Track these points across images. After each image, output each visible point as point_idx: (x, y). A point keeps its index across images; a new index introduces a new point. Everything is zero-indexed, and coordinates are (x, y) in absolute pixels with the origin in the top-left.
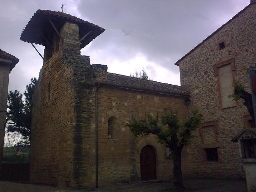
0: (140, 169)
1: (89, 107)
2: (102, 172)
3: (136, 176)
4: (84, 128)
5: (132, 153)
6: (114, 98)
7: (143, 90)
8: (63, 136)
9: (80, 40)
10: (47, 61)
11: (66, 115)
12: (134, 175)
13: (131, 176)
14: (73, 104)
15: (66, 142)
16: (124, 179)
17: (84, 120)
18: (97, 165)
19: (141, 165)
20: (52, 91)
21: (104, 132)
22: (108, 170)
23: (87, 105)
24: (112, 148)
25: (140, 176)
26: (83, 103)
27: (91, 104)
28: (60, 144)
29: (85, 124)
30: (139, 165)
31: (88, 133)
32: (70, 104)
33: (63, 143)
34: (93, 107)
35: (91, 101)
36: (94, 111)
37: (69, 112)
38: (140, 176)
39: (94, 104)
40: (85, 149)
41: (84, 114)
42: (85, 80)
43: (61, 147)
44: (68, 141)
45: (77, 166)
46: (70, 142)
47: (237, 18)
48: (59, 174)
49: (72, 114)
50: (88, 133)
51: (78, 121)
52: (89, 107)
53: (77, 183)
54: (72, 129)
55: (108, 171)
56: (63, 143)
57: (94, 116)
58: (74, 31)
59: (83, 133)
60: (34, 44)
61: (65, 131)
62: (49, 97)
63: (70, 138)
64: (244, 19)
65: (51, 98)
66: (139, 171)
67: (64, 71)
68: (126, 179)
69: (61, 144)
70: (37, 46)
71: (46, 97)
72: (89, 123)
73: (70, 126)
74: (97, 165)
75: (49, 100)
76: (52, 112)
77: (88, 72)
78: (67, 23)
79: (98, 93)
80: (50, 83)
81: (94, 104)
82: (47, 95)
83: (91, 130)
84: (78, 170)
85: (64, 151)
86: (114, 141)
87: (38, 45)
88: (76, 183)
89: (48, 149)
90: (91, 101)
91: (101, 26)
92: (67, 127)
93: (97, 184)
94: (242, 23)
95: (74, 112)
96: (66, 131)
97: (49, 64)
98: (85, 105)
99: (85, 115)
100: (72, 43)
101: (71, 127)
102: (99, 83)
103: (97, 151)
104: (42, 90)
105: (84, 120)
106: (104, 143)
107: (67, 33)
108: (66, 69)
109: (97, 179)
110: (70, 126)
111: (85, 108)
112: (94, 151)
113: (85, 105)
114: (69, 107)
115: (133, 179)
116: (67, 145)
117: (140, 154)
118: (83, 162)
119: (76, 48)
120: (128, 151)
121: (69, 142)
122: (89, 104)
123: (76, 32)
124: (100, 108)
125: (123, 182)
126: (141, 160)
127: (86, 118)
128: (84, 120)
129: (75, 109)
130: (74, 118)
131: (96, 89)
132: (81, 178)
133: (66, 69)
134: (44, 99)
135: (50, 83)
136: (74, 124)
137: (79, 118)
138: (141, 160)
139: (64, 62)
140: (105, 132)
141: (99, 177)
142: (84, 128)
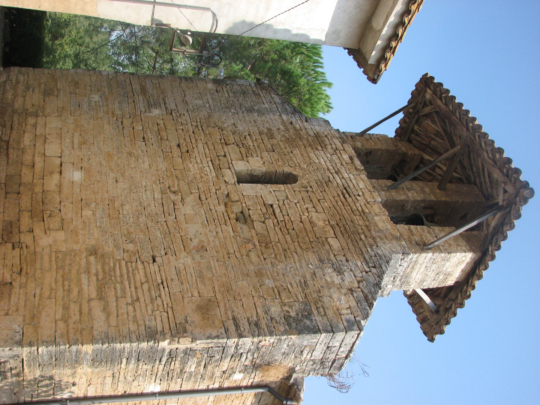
23: (225, 369)
31: (130, 379)
32: (234, 319)
60: (401, 115)
89: (78, 176)
128: (177, 365)
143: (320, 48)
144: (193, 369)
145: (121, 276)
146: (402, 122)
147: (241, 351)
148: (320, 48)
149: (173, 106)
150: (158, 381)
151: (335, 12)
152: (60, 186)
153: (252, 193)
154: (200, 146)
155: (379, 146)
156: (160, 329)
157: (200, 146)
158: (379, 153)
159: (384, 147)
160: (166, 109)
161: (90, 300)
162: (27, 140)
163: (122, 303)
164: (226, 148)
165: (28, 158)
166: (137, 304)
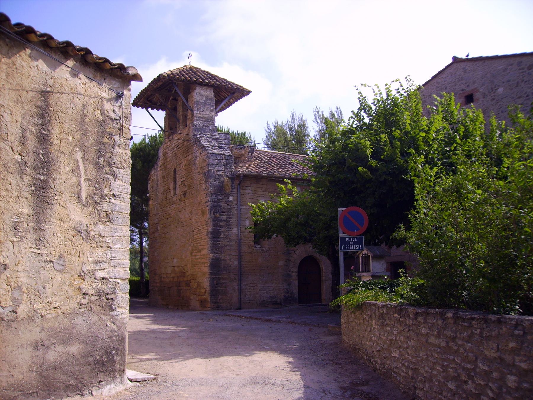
0: (297, 288)
1: (229, 207)
2: (246, 291)
3: (291, 297)
4: (222, 233)
5: (287, 266)
6: (262, 193)
7: (229, 315)
8: (196, 244)
9: (216, 108)
10: (171, 138)
11: (200, 216)
12: (288, 296)
13: (285, 296)
14: (209, 203)
15: (200, 251)
16: (275, 300)
17: (222, 224)
18: (240, 280)
19: (298, 283)
20: (179, 182)
21: (248, 238)
22: (255, 288)
23: (226, 204)
24: (260, 260)
25: (297, 297)
26: (222, 202)
27: (231, 202)
28: (191, 254)
29: (224, 229)
30: (296, 282)
31: (229, 240)
32: (205, 203)
33: (196, 252)
34: (235, 206)
35: (231, 198)
36: (236, 212)
37: (203, 213)
38: (296, 296)
39: (236, 202)
40: (225, 260)
41: (223, 215)
42: (224, 170)
43: (194, 257)
44: (203, 250)
45: (215, 282)
46: (205, 252)
47: (436, 79)
48: (191, 292)
49: (208, 216)
50: (229, 240)
51: (216, 225)
52: (229, 207)
53: (215, 303)
54: (207, 235)
55: (254, 289)
56: (196, 252)
57: (235, 218)
58: (207, 98)
59: (221, 240)
60: (150, 109)
61: (198, 237)
62: (175, 188)
63: (205, 247)
64: (445, 82)
65: (178, 191)
66: (295, 290)
67: (196, 157)
68: (278, 300)
69: (193, 254)
70: (154, 112)
71: (170, 188)
72: (229, 226)
73: (205, 231)
74: (240, 280)
75: (175, 194)
76: (180, 210)
77: (227, 160)
78: (197, 88)
79: (242, 187)
80: (175, 169)
81: (236, 202)
82: (171, 186)
83: (232, 236)
84: (216, 287)
85: (198, 263)
86: (262, 250)
87: (155, 110)
88: (213, 302)
89: (175, 260)
90: (231, 198)
91: (245, 85)
92: (201, 233)
93: (240, 304)
94: (442, 87)
95: (211, 213)
96: (200, 237)
97: (174, 142)
98: (223, 204)
99: (223, 217)
100: (206, 116)
101: (206, 233)
102: (242, 175)
103: (240, 262)
104: (163, 177)
105: (222, 224)
106: (248, 253)
107: (198, 101)
108: (198, 154)
109: (240, 298)
110: (205, 231)
111: (224, 208)
112: (236, 263)
113: (224, 204)
114: (203, 207)
115: (288, 300)
116: (201, 255)
117: (297, 267)
118: (222, 276)
119: (211, 123)
120: (281, 263)
121: (205, 252)
122: (228, 202)
123: (211, 99)
124: (244, 207)
125: (273, 304)
126: (298, 276)
127: (225, 221)
128: (223, 223)
129: (211, 209)
130: (210, 221)
131: (238, 183)
132: (220, 297)
133: (198, 154)
134: (167, 191)
135: (175, 169)
136: (210, 229)
137: (216, 221)
138: (299, 276)
139: (195, 144)
140: (250, 239)
141: (242, 296)
142: (222, 233)
143: (151, 136)
144: (225, 217)
145: (196, 244)
146: (153, 109)
147: (216, 200)
148: (151, 136)
149: (157, 220)
150: (231, 229)
151: (230, 83)
152: (178, 267)
153: (179, 189)
154: (167, 209)
155: (167, 123)
156: (206, 231)
157: (167, 209)
158: (170, 123)
159: (168, 121)
160: (158, 223)
161: (201, 255)
162: (167, 280)
163: (202, 243)
164: (168, 198)
165: (172, 279)
166: (202, 238)
